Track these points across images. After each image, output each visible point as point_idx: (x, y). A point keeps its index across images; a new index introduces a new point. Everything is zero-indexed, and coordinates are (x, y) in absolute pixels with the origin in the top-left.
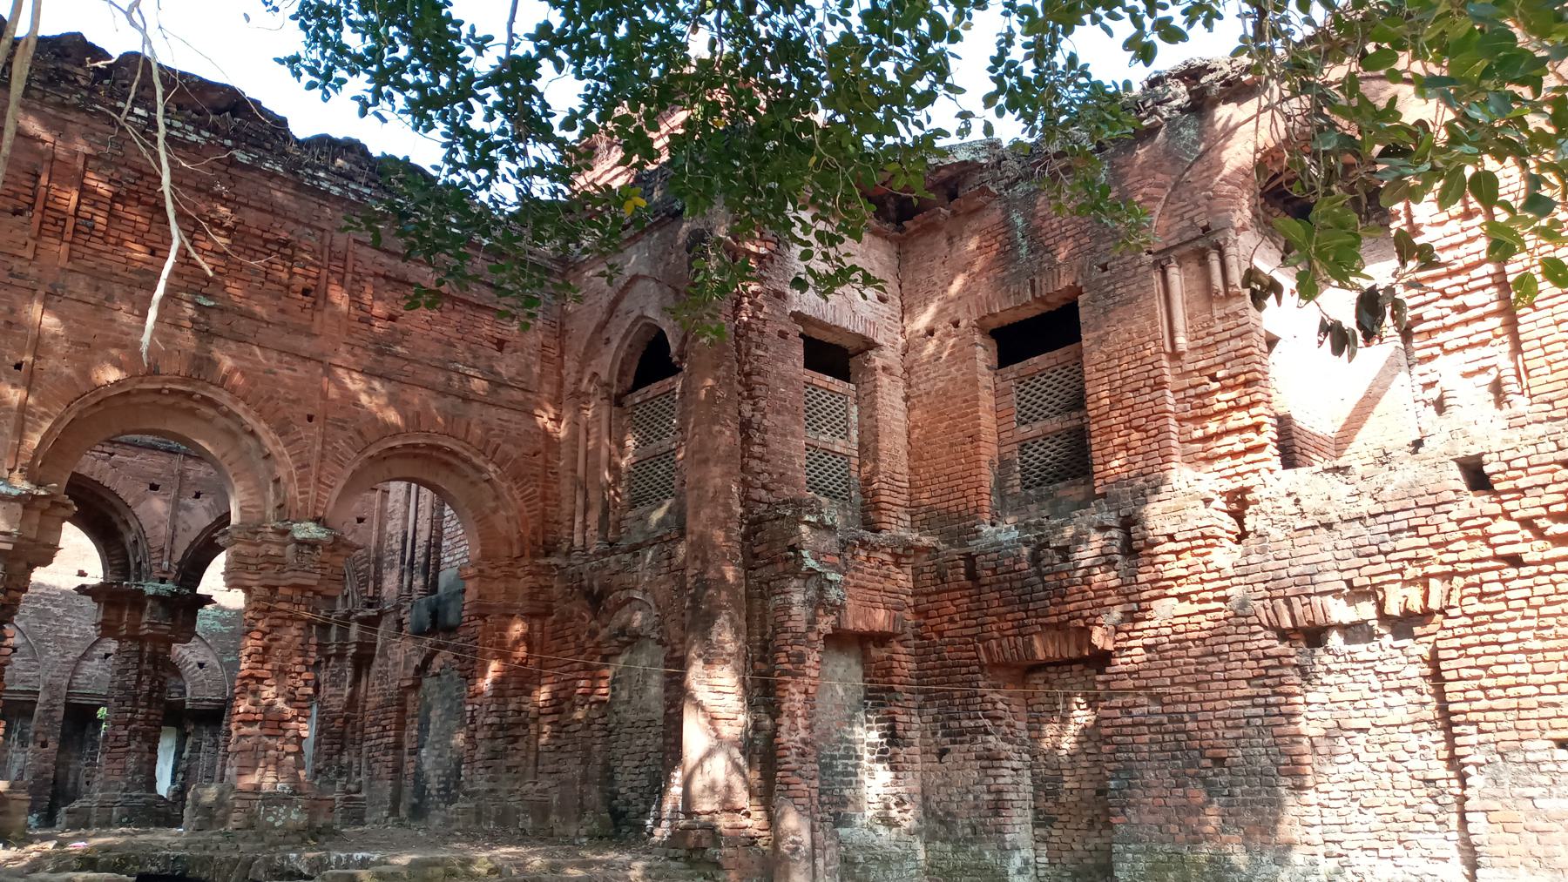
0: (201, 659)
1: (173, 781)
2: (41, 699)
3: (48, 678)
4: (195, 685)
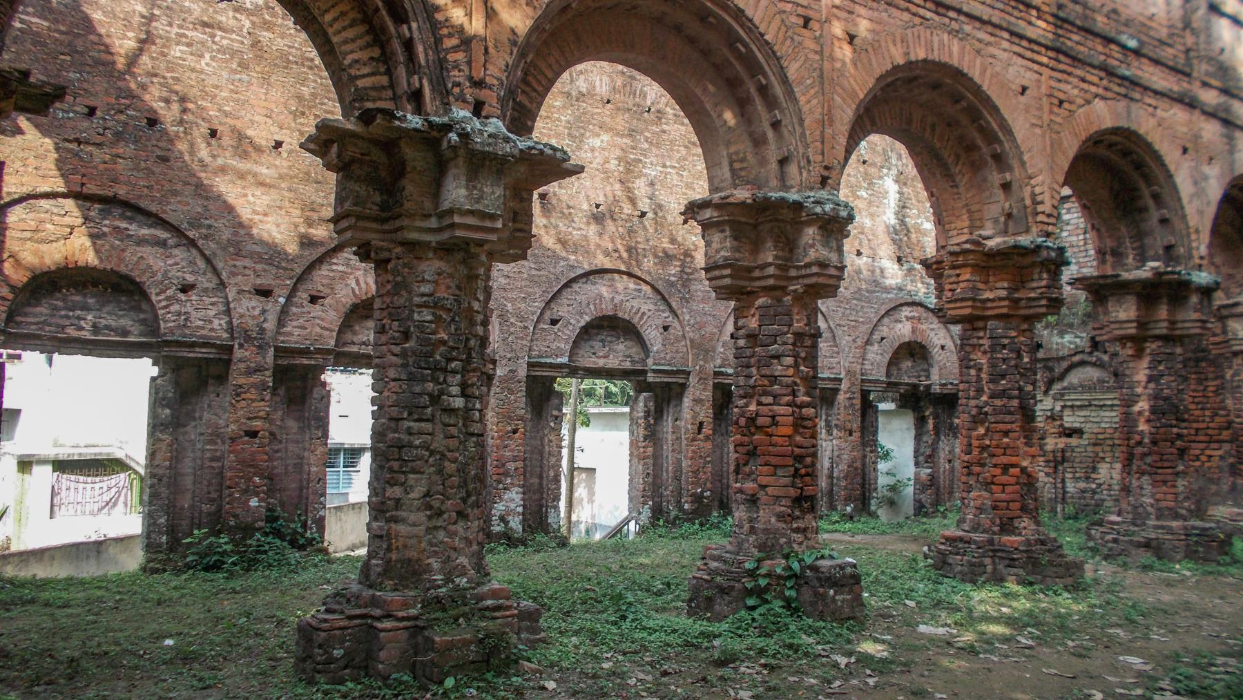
0: (942, 342)
1: (917, 464)
2: (844, 386)
3: (847, 365)
4: (941, 369)
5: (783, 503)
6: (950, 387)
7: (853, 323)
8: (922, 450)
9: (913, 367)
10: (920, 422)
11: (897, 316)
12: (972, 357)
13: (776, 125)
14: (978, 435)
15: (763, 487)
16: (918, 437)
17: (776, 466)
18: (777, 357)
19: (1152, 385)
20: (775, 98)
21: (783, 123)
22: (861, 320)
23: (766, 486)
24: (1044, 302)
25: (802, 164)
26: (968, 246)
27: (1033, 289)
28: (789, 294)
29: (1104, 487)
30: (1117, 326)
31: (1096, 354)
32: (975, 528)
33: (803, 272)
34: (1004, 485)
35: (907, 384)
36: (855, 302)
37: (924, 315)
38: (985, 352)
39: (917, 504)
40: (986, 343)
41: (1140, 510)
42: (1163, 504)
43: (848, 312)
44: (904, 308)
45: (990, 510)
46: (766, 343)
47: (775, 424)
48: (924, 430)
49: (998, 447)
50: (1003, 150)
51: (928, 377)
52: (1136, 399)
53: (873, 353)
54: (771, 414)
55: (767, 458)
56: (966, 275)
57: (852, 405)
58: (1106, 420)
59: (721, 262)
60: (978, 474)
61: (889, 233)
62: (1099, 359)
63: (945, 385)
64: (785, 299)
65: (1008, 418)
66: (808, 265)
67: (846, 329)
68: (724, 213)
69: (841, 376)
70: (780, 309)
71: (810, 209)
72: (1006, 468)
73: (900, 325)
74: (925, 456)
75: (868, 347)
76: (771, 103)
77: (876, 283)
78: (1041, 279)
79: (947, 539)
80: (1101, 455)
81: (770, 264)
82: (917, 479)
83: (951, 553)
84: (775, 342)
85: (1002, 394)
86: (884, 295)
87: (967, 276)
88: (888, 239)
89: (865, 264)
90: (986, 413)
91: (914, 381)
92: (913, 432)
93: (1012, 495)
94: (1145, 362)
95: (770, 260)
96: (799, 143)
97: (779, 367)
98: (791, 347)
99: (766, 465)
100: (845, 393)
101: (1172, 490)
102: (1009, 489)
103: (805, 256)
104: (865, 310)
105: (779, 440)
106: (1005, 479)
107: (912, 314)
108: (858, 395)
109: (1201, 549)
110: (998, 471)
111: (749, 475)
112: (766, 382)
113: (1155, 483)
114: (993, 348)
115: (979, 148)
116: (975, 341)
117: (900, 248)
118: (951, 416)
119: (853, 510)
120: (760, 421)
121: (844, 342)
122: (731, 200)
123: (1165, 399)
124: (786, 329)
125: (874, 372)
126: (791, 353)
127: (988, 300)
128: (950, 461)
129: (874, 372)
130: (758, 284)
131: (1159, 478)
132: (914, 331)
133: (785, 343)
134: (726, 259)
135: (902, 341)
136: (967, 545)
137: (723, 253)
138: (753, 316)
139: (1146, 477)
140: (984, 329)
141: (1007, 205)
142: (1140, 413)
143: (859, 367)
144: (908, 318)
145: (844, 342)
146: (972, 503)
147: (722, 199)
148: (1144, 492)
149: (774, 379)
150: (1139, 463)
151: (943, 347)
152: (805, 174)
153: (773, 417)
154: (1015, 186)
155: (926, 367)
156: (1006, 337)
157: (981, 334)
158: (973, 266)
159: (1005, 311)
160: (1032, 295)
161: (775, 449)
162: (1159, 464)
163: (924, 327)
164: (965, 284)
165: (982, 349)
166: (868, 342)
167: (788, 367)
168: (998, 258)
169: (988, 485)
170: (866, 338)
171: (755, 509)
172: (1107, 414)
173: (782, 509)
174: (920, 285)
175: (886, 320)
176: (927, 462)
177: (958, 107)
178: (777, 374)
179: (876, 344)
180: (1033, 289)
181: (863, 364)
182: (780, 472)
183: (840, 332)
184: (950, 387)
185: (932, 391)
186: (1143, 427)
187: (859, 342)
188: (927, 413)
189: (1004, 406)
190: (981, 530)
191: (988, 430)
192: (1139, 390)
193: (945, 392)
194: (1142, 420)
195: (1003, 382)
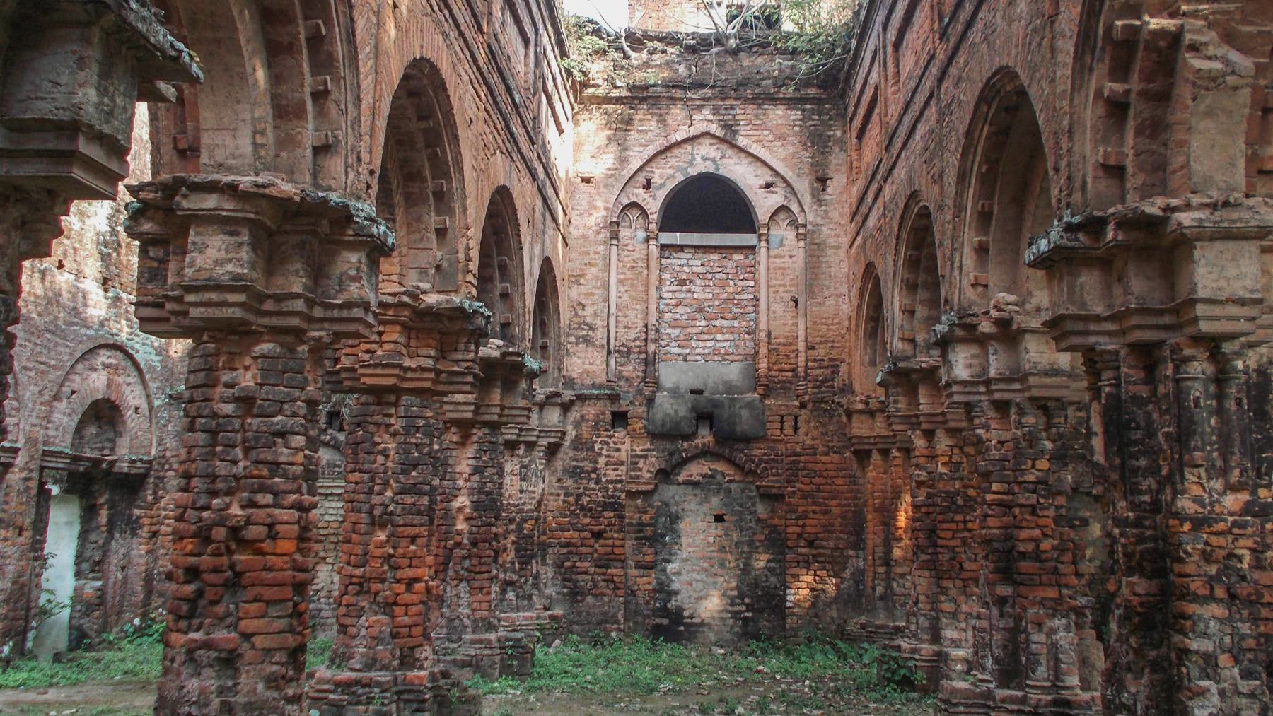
1: (78, 575)
2: (20, 460)
3: (28, 428)
5: (277, 658)
6: (139, 464)
7: (42, 367)
8: (88, 554)
9: (97, 435)
10: (89, 514)
11: (92, 362)
12: (377, 439)
13: (320, 96)
14: (376, 542)
15: (247, 636)
16: (83, 536)
17: (268, 603)
18: (282, 434)
19: (476, 478)
20: (331, 58)
21: (332, 97)
22: (53, 362)
23: (253, 635)
24: (470, 379)
25: (350, 160)
26: (406, 299)
27: (457, 362)
28: (304, 343)
29: (324, 593)
30: (451, 407)
31: (330, 431)
32: (370, 665)
33: (336, 314)
34: (407, 605)
35: (89, 459)
36: (48, 335)
37: (123, 363)
38: (394, 435)
39: (75, 633)
40: (398, 424)
41: (457, 623)
42: (478, 614)
43: (38, 349)
44: (103, 352)
45: (389, 639)
46: (270, 410)
47: (273, 536)
48: (94, 524)
49: (404, 556)
50: (450, 190)
51: (113, 450)
52: (456, 492)
53: (60, 412)
54: (269, 520)
55: (257, 590)
56: (394, 334)
57: (28, 489)
58: (331, 511)
59: (226, 280)
60: (377, 594)
61: (98, 244)
62: (333, 438)
63: (134, 462)
64: (300, 349)
65: (417, 519)
66: (348, 305)
67: (32, 374)
68: (248, 207)
69: (18, 445)
70: (291, 363)
71: (363, 227)
72: (411, 583)
73: (94, 375)
74: (87, 564)
75: (56, 404)
76: (322, 62)
77: (75, 312)
78: (467, 350)
79: (338, 684)
80: (322, 554)
81: (298, 296)
82: (77, 597)
83: (349, 703)
84: (280, 412)
85: (413, 489)
86: (83, 331)
87: (395, 337)
88: (95, 252)
89: (67, 282)
90: (391, 514)
91: (96, 455)
92: (77, 529)
93: (415, 618)
94: (471, 451)
95: (297, 289)
96: (350, 131)
97: (285, 451)
98: (303, 421)
99: (255, 600)
100: (22, 470)
101: (487, 598)
102: (413, 609)
103: (341, 291)
104: (59, 349)
105: (279, 561)
106: (407, 597)
107: (110, 361)
108: (35, 475)
109: (515, 663)
110: (401, 588)
111: (221, 619)
112: (265, 472)
113: (472, 591)
114: (410, 429)
115: (424, 180)
116: (379, 418)
117: (107, 267)
118: (131, 505)
119: (12, 650)
120: (254, 532)
121: (28, 394)
122: (271, 191)
123: (489, 494)
124: (297, 393)
125: (57, 441)
126: (302, 430)
127: (410, 369)
128: (123, 568)
129: (57, 441)
130: (266, 321)
131: (477, 584)
132: (109, 384)
133: (295, 415)
134: (237, 277)
135: (95, 398)
136: (367, 690)
137: (230, 267)
138: (247, 368)
139: (463, 584)
140: (396, 405)
141: (439, 254)
142: (460, 509)
143: (42, 432)
144: (106, 366)
145: (28, 394)
146: (363, 632)
147: (257, 186)
148: (461, 602)
149: (275, 466)
150: (458, 568)
151: (137, 409)
152: (351, 175)
153: (271, 526)
154: (450, 235)
155: (111, 435)
156: (421, 417)
157: (392, 411)
158: (404, 326)
159: (428, 384)
160: (456, 369)
161: (270, 575)
162: (477, 569)
163: (120, 380)
164: (392, 346)
165: (391, 430)
166: (56, 397)
167: (298, 450)
168: (428, 319)
169: (388, 607)
170: (55, 389)
171: (229, 673)
172: (334, 504)
173: (275, 668)
174: (124, 322)
175: (80, 366)
176: (92, 571)
177: (423, 125)
178: (282, 459)
179: (65, 401)
180: (457, 362)
181: (47, 428)
182: (273, 611)
183: (25, 379)
184: (139, 464)
185: (116, 470)
186: (461, 526)
187: (47, 396)
188: (102, 501)
189: (414, 504)
190: (378, 665)
191: (392, 535)
192: (461, 483)
193: (133, 471)
194: (461, 517)
195: (414, 474)
